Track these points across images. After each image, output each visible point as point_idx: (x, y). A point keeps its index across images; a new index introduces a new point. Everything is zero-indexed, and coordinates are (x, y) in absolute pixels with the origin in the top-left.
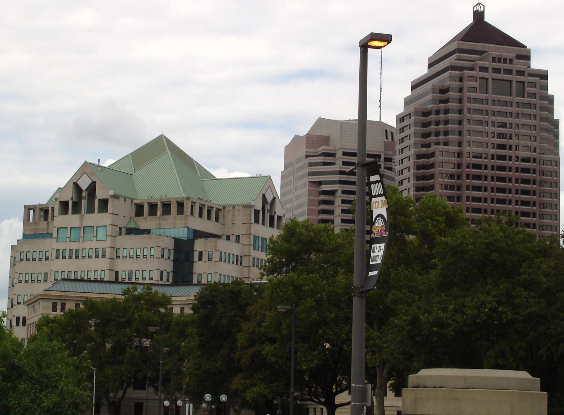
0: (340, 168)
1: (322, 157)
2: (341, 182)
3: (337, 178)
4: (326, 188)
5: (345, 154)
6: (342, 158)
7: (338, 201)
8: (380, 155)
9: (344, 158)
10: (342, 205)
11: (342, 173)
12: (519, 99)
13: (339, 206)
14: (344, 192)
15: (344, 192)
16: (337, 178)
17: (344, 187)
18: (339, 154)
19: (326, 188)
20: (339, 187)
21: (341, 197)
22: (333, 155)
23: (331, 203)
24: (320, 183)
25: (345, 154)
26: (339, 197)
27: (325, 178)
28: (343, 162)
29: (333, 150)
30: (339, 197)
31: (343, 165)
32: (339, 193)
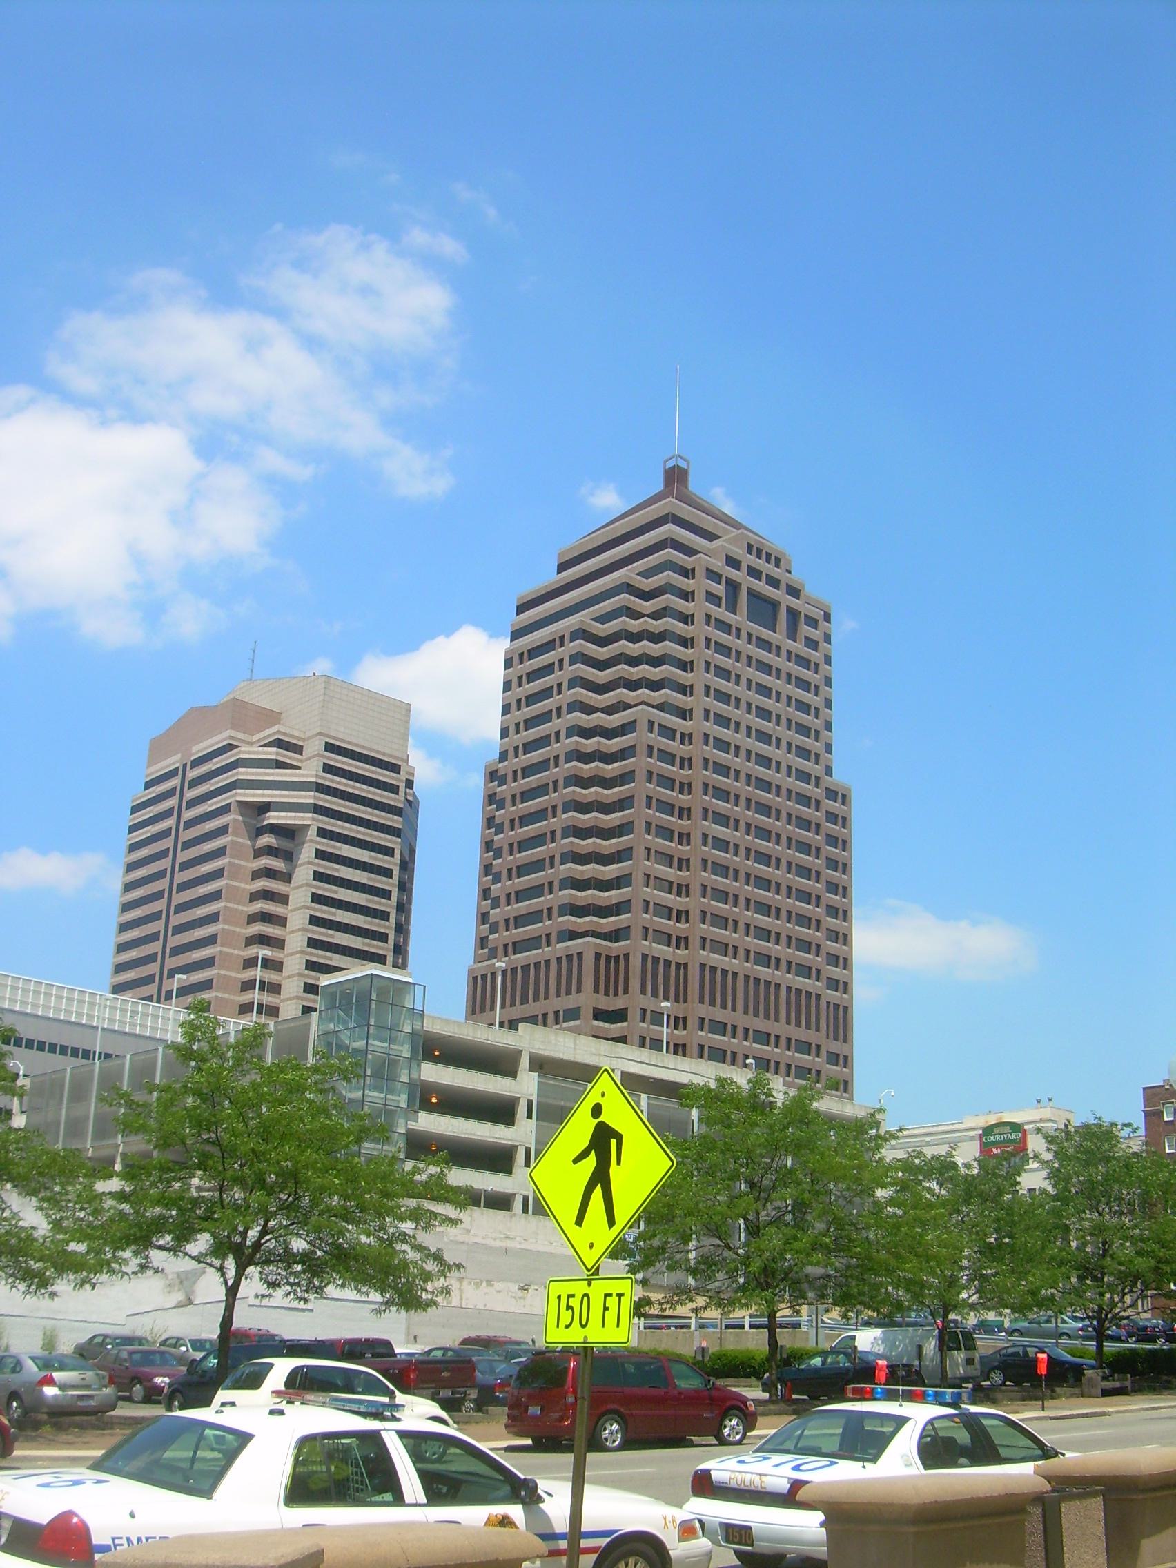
0: (317, 776)
1: (274, 749)
2: (318, 809)
3: (308, 797)
4: (278, 818)
5: (330, 747)
6: (308, 931)
7: (307, 853)
8: (387, 935)
9: (313, 932)
10: (307, 972)
11: (320, 788)
12: (704, 1010)
13: (309, 863)
14: (322, 833)
15: (322, 833)
16: (308, 797)
17: (323, 844)
18: (314, 747)
19: (278, 818)
20: (313, 819)
21: (316, 842)
22: (298, 749)
23: (289, 856)
24: (265, 808)
25: (330, 747)
26: (311, 841)
27: (276, 796)
28: (307, 961)
29: (299, 739)
30: (311, 841)
31: (316, 857)
32: (312, 833)
